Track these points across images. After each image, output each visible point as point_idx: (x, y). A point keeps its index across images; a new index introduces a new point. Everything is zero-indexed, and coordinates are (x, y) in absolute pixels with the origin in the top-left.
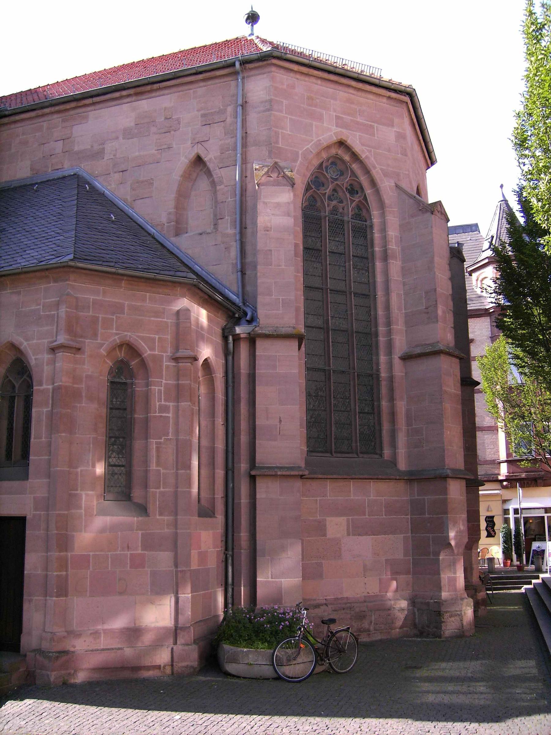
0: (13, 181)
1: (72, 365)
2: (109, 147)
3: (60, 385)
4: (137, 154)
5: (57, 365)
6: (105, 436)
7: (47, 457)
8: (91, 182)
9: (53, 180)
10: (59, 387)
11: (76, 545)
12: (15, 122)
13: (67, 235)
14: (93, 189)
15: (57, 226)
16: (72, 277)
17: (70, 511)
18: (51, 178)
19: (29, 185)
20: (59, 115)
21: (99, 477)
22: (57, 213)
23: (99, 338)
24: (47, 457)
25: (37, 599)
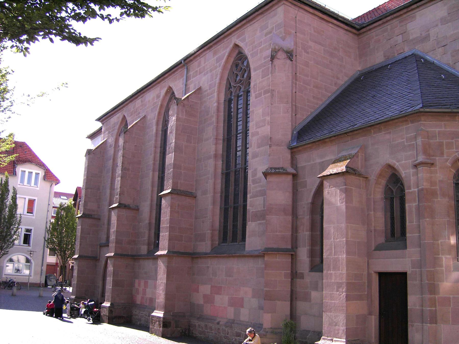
0: (374, 65)
1: (429, 175)
2: (433, 32)
3: (422, 188)
4: (452, 32)
5: (419, 175)
6: (455, 219)
7: (418, 234)
8: (423, 57)
9: (399, 60)
10: (422, 190)
11: (441, 291)
12: (370, 30)
13: (415, 93)
14: (426, 60)
15: (408, 88)
16: (423, 118)
17: (436, 269)
18: (398, 60)
19: (385, 66)
20: (397, 19)
21: (452, 246)
22: (406, 80)
23: (445, 156)
24: (418, 234)
25: (417, 325)
